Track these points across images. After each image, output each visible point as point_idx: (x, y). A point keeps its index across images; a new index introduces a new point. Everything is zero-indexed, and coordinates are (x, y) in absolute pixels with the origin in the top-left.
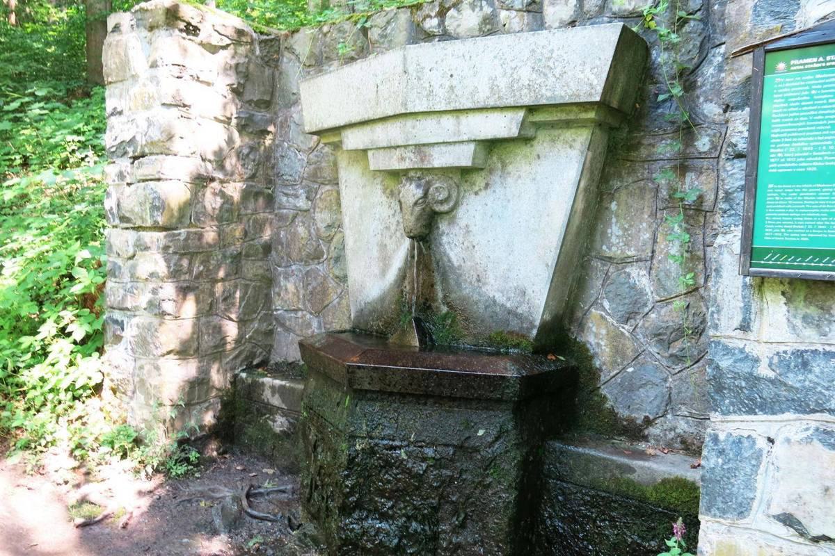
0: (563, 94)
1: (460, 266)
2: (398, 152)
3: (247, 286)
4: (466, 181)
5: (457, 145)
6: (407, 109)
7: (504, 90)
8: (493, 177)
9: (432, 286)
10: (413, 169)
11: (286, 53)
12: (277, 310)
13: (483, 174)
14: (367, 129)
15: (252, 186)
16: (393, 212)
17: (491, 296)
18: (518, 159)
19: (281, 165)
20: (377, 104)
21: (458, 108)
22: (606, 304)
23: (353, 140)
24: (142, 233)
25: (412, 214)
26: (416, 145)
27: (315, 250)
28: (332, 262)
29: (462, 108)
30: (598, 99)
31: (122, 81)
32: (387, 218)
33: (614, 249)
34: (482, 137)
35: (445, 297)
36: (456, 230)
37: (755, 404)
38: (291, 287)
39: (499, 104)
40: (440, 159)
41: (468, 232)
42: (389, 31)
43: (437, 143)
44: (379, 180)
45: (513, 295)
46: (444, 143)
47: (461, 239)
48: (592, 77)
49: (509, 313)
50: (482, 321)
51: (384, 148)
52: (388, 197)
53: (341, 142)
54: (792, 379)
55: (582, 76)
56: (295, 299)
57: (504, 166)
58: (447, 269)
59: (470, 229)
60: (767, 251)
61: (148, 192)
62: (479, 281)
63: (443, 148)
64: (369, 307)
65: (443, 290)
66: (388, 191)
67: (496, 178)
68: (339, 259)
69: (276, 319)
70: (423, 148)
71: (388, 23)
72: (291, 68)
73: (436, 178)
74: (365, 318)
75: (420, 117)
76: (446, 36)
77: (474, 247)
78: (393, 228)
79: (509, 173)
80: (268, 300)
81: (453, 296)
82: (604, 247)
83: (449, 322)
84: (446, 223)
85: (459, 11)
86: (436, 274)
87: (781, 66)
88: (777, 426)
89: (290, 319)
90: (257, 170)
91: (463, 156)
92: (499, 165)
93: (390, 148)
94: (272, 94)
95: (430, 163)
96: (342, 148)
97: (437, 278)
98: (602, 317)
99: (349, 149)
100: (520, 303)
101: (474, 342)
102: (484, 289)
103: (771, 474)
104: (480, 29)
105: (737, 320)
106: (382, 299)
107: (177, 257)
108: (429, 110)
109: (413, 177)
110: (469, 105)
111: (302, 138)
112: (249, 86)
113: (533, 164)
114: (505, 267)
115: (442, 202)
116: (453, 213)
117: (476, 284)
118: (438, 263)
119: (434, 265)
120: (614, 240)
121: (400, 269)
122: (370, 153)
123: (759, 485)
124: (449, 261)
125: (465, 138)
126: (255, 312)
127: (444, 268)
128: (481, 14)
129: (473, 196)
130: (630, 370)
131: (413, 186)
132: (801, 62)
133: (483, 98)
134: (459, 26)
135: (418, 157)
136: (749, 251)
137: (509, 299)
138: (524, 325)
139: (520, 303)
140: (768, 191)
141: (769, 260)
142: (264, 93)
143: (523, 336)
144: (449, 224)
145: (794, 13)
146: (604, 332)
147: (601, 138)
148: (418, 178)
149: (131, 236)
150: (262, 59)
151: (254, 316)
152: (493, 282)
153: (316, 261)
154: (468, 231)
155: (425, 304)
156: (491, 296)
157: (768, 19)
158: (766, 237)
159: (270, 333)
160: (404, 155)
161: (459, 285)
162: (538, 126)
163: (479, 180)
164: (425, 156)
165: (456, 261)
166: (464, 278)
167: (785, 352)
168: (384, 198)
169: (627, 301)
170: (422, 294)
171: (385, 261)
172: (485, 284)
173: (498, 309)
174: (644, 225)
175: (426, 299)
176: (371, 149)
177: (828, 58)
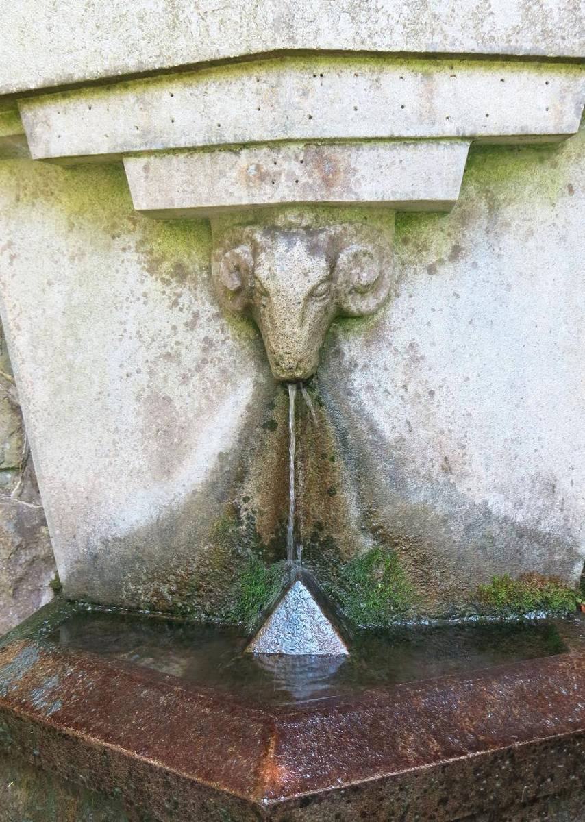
1: (401, 440)
4: (405, 241)
5: (423, 147)
6: (292, 39)
7: (555, 15)
8: (470, 234)
9: (331, 492)
10: (293, 205)
13: (445, 223)
16: (187, 317)
17: (479, 501)
18: (526, 193)
20: (173, 27)
21: (439, 49)
23: (62, 131)
25: (302, 323)
26: (308, 142)
29: (450, 49)
32: (168, 331)
35: (367, 515)
36: (386, 356)
39: (543, 48)
40: (376, 180)
41: (416, 360)
43: (368, 140)
44: (131, 240)
45: (528, 495)
46: (392, 139)
47: (400, 378)
49: (521, 536)
50: (462, 559)
51: (192, 150)
52: (166, 282)
53: (22, 137)
57: (493, 208)
58: (368, 447)
59: (421, 352)
62: (447, 470)
63: (385, 153)
64: (120, 550)
65: (361, 500)
66: (166, 266)
67: (475, 234)
70: (328, 151)
73: (351, 229)
74: (109, 575)
75: (322, 67)
77: (432, 393)
78: (190, 358)
79: (507, 224)
81: (387, 510)
83: (380, 571)
84: (360, 340)
86: (339, 463)
91: (437, 175)
92: (483, 205)
93: (209, 149)
95: (348, 189)
96: (27, 154)
97: (342, 472)
99: (56, 152)
100: (545, 511)
101: (445, 609)
102: (461, 489)
106: (165, 529)
108: (358, 47)
109: (291, 226)
110: (468, 45)
113: (559, 204)
114: (509, 434)
116: (376, 318)
117: (441, 479)
118: (343, 437)
119: (334, 443)
121: (222, 457)
122: (133, 168)
124: (373, 429)
125: (450, 129)
127: (361, 449)
129: (424, 276)
131: (299, 249)
135: (316, 175)
137: (519, 504)
138: (556, 557)
139: (545, 511)
143: (556, 581)
144: (368, 343)
148: (307, 228)
152: (481, 470)
154: (414, 357)
155: (315, 537)
156: (479, 501)
160: (268, 167)
161: (400, 485)
163: (438, 238)
164: (336, 172)
165: (388, 430)
166: (411, 466)
168: (152, 285)
170: (306, 514)
171: (169, 440)
172: (463, 476)
173: (495, 529)
175: (319, 526)
176: (137, 154)
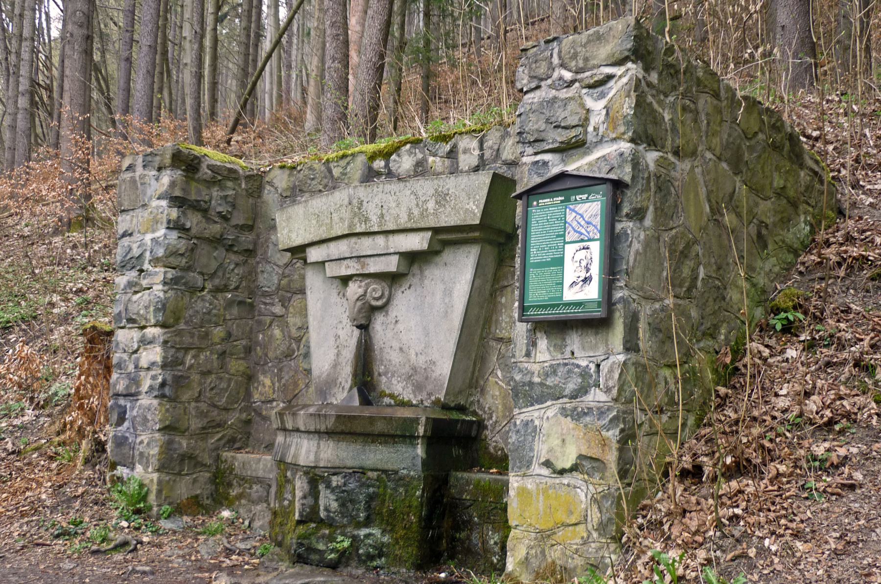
3: (230, 380)
11: (268, 187)
12: (255, 403)
14: (324, 246)
15: (237, 296)
22: (499, 373)
27: (288, 349)
28: (301, 358)
30: (478, 222)
34: (403, 250)
38: (268, 382)
40: (374, 267)
54: (549, 382)
55: (468, 207)
56: (271, 391)
57: (422, 272)
61: (152, 297)
68: (307, 355)
69: (255, 410)
70: (362, 259)
72: (270, 196)
80: (248, 395)
85: (399, 156)
88: (543, 411)
90: (241, 282)
91: (391, 265)
94: (254, 220)
98: (496, 382)
104: (415, 171)
105: (524, 353)
107: (174, 350)
111: (278, 255)
112: (235, 213)
115: (377, 299)
122: (326, 264)
123: (536, 448)
125: (392, 251)
126: (236, 402)
128: (415, 159)
133: (404, 221)
134: (399, 167)
142: (247, 219)
150: (247, 191)
151: (236, 406)
153: (289, 359)
159: (248, 422)
162: (446, 244)
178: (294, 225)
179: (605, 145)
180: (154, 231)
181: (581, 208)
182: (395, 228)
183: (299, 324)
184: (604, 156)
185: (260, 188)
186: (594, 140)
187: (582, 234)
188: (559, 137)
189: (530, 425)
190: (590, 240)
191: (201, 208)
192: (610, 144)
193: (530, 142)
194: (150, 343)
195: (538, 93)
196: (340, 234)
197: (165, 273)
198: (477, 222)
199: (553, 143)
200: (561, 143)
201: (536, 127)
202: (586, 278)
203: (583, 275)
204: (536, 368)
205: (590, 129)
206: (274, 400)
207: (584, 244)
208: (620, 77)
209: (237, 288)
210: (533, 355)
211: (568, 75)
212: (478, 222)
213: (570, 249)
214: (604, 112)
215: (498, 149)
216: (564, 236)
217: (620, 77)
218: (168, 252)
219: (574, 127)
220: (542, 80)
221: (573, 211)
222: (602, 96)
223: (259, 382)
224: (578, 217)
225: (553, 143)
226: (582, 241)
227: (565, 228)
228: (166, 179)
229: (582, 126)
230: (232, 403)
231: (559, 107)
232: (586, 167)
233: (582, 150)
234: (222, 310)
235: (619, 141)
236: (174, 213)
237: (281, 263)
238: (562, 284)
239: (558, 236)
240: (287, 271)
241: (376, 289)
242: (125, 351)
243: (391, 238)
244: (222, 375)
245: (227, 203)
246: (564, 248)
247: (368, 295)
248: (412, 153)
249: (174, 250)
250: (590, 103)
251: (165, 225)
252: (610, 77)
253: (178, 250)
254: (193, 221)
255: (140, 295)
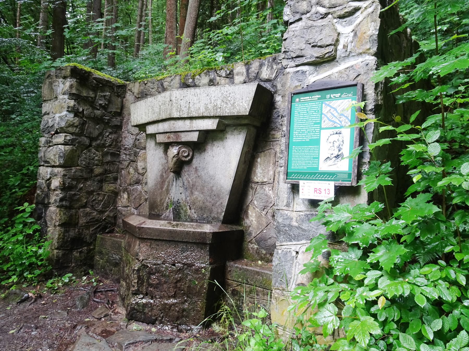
0: (235, 112)
2: (168, 134)
11: (129, 92)
19: (124, 141)
23: (151, 129)
24: (54, 169)
31: (50, 100)
33: (259, 178)
34: (202, 129)
37: (292, 237)
40: (185, 138)
42: (172, 84)
48: (245, 105)
54: (305, 226)
60: (293, 173)
61: (58, 149)
71: (172, 80)
72: (129, 97)
76: (195, 86)
80: (115, 202)
82: (255, 178)
87: (297, 100)
88: (299, 246)
89: (124, 211)
90: (112, 143)
91: (194, 137)
103: (297, 266)
105: (285, 203)
120: (259, 175)
122: (157, 135)
126: (108, 207)
130: (265, 231)
132: (304, 98)
136: (286, 173)
140: (294, 149)
141: (293, 176)
145: (305, 80)
146: (254, 215)
147: (253, 130)
149: (49, 170)
154: (196, 169)
157: (296, 81)
158: (293, 167)
167: (302, 215)
169: (264, 201)
174: (271, 168)
177: (313, 97)
178: (140, 112)
179: (352, 59)
180: (60, 113)
181: (335, 104)
182: (197, 115)
183: (144, 167)
184: (352, 66)
185: (125, 92)
186: (343, 55)
187: (335, 122)
188: (313, 54)
189: (289, 254)
190: (341, 127)
191: (91, 103)
192: (356, 58)
193: (292, 58)
194: (56, 175)
195: (300, 23)
196: (164, 118)
197: (66, 136)
198: (147, 127)
199: (311, 57)
200: (317, 57)
201: (298, 47)
202: (338, 155)
203: (336, 153)
204: (294, 215)
205: (340, 47)
206: (128, 206)
207: (337, 130)
208: (366, 8)
209: (110, 146)
210: (291, 206)
211: (323, 10)
212: (247, 114)
213: (324, 134)
214: (352, 34)
215: (258, 72)
216: (320, 123)
217: (366, 8)
218: (67, 124)
219: (328, 46)
220: (303, 14)
221: (328, 105)
222: (350, 23)
223: (121, 196)
224: (332, 110)
225: (311, 57)
226: (335, 127)
227: (321, 118)
228: (68, 84)
229: (334, 45)
230: (105, 208)
231: (316, 32)
232: (336, 75)
233: (333, 63)
234: (101, 157)
235: (364, 55)
236: (72, 103)
237: (134, 133)
238: (318, 158)
239: (315, 123)
240: (138, 137)
241: (185, 151)
242: (43, 179)
243: (194, 121)
244: (100, 192)
245: (105, 99)
246: (320, 132)
247: (180, 154)
248: (207, 75)
249: (71, 123)
250: (340, 28)
251: (66, 109)
252: (356, 10)
253: (74, 123)
254: (84, 108)
255: (52, 148)
